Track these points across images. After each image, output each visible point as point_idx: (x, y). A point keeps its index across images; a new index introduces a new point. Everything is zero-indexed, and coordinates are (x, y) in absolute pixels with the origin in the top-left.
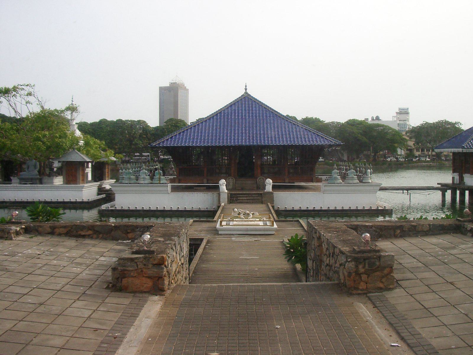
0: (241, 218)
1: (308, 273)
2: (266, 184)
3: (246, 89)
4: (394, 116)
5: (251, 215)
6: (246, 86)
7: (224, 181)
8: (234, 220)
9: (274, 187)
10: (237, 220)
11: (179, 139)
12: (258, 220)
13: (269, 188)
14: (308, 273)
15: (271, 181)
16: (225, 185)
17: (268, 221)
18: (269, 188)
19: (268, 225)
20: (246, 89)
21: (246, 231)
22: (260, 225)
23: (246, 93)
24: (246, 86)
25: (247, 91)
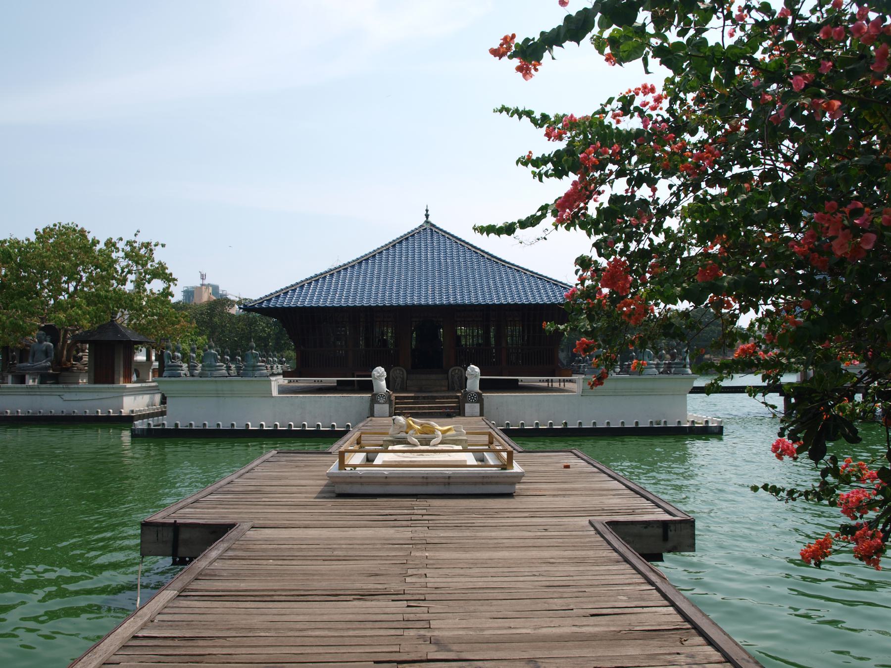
0: (408, 443)
1: (798, 485)
2: (468, 377)
3: (427, 216)
4: (713, 443)
5: (440, 433)
6: (427, 211)
7: (383, 369)
8: (390, 448)
9: (486, 386)
10: (397, 447)
11: (344, 279)
12: (460, 448)
13: (473, 385)
14: (798, 485)
15: (477, 369)
16: (384, 378)
17: (486, 451)
18: (473, 385)
19: (492, 463)
20: (427, 216)
21: (423, 484)
22: (468, 463)
23: (427, 222)
24: (427, 211)
25: (430, 219)
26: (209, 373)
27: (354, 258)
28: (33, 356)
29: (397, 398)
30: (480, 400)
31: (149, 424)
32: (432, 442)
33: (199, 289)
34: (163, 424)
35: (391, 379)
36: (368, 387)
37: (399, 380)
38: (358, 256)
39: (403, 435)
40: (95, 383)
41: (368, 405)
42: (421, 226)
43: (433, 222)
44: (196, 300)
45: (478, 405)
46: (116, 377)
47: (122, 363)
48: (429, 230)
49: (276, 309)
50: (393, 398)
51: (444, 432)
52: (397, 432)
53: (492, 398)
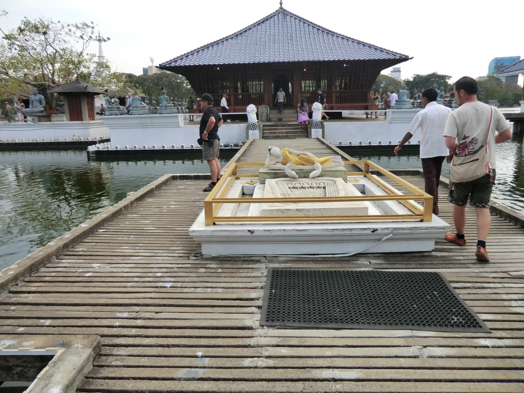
2: (314, 111)
3: (281, 4)
13: (317, 116)
15: (320, 105)
16: (255, 112)
18: (317, 116)
20: (281, 4)
23: (281, 8)
25: (283, 6)
26: (136, 112)
27: (233, 33)
28: (32, 104)
29: (264, 126)
30: (323, 127)
31: (98, 148)
32: (311, 175)
33: (150, 67)
34: (108, 147)
35: (259, 113)
36: (244, 118)
37: (265, 114)
38: (236, 32)
39: (280, 166)
40: (71, 120)
41: (244, 131)
42: (277, 11)
43: (285, 8)
44: (150, 73)
45: (320, 130)
46: (83, 116)
47: (86, 107)
48: (282, 12)
49: (180, 67)
50: (261, 126)
51: (322, 163)
52: (273, 162)
53: (331, 126)
